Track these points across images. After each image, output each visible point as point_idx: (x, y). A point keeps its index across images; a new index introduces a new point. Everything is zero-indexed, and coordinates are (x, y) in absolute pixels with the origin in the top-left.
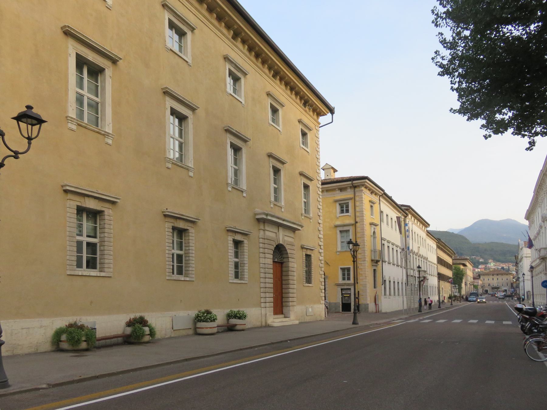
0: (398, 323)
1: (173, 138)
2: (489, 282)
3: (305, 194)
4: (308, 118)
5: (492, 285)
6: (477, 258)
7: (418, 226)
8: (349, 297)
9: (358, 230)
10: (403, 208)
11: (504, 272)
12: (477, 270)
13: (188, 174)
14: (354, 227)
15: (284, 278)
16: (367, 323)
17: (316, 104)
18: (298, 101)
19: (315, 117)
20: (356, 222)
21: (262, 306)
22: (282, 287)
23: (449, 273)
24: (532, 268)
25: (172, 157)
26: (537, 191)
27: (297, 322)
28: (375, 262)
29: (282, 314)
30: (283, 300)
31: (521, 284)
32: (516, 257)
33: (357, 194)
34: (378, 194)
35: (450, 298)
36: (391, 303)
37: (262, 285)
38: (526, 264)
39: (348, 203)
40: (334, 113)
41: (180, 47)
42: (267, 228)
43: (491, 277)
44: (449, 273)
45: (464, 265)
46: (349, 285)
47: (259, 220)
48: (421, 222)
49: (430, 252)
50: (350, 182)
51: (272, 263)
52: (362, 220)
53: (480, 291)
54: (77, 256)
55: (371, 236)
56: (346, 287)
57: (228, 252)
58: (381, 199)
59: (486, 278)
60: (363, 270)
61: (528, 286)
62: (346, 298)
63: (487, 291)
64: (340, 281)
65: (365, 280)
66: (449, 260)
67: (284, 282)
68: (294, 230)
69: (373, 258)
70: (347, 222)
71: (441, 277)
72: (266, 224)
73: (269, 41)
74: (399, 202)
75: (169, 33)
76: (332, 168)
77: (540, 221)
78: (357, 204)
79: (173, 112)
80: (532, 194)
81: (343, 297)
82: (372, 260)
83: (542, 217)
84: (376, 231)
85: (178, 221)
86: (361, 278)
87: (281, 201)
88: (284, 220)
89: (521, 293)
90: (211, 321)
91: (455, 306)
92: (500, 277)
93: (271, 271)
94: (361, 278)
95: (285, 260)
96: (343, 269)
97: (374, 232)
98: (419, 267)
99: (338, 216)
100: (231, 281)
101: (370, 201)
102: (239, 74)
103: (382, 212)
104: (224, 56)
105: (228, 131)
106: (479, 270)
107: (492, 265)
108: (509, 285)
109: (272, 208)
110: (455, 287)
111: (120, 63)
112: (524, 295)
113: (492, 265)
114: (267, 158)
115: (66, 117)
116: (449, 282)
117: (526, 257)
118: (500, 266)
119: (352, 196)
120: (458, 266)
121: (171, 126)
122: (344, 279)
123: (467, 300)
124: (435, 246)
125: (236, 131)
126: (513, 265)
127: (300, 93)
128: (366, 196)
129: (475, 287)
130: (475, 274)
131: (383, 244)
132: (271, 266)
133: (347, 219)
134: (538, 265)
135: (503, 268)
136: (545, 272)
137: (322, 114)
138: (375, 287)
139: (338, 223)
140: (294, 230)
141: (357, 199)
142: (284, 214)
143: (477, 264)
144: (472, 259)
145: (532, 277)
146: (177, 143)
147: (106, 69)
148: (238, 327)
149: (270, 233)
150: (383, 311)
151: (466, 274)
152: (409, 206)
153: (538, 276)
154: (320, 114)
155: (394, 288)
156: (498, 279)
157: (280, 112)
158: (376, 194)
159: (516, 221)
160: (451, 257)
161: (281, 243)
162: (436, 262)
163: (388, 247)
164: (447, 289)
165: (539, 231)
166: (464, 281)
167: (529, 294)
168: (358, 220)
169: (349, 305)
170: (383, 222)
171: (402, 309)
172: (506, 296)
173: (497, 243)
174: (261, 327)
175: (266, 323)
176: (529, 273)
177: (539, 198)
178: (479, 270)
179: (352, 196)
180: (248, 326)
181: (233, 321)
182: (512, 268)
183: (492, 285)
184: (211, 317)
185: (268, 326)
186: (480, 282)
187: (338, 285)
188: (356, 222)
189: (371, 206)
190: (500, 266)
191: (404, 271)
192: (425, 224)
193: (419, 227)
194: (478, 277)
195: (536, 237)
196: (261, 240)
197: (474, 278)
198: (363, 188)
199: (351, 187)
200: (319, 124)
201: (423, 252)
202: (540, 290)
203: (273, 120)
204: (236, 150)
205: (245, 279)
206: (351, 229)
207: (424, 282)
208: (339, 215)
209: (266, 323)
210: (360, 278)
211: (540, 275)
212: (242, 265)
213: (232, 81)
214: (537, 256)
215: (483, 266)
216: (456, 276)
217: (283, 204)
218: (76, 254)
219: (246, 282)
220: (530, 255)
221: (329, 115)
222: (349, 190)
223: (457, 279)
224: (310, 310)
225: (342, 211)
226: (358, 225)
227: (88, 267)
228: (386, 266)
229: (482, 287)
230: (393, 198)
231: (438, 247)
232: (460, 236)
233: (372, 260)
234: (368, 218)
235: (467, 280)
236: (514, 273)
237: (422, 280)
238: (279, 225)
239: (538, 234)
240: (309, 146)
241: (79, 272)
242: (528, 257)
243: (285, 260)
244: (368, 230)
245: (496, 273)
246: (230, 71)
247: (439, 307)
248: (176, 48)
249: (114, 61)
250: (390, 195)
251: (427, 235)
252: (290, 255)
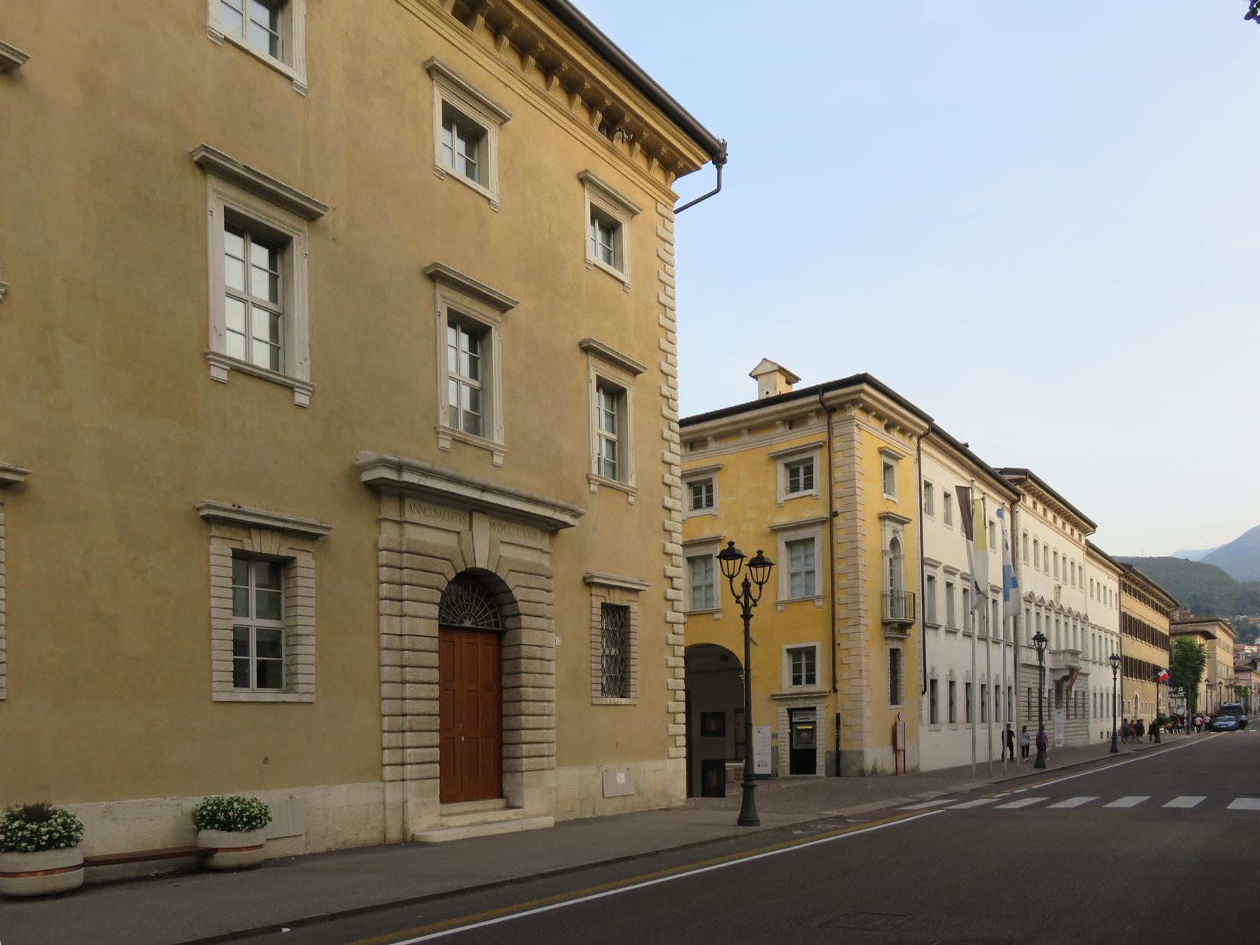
0: (926, 808)
1: (457, 381)
4: (622, 172)
7: (1057, 530)
8: (812, 732)
9: (840, 535)
10: (1006, 477)
12: (1248, 649)
14: (826, 528)
15: (507, 681)
16: (784, 819)
17: (660, 134)
18: (581, 114)
19: (658, 175)
21: (387, 776)
22: (501, 709)
23: (1159, 657)
27: (549, 821)
29: (500, 794)
33: (836, 432)
34: (913, 434)
36: (942, 746)
37: (386, 707)
40: (724, 161)
41: (273, 39)
44: (1159, 657)
45: (1208, 636)
46: (811, 696)
47: (376, 490)
48: (1067, 519)
49: (1102, 604)
50: (816, 398)
51: (436, 633)
54: (235, 661)
55: (884, 552)
58: (923, 445)
60: (852, 652)
62: (804, 735)
64: (787, 686)
65: (856, 682)
66: (1161, 624)
67: (506, 695)
68: (551, 528)
69: (889, 617)
70: (808, 514)
71: (1131, 668)
72: (407, 503)
73: (634, 74)
74: (994, 462)
76: (782, 370)
78: (838, 459)
82: (885, 624)
87: (491, 432)
88: (484, 489)
90: (39, 848)
93: (434, 659)
94: (846, 675)
95: (510, 623)
96: (795, 653)
97: (894, 543)
98: (1039, 638)
99: (780, 500)
100: (216, 697)
101: (882, 452)
103: (928, 485)
105: (207, 166)
109: (444, 451)
110: (1176, 693)
111: (327, 218)
114: (423, 286)
115: (207, 354)
116: (1157, 680)
119: (823, 437)
120: (1188, 638)
121: (451, 352)
122: (797, 681)
123: (1210, 727)
125: (247, 168)
127: (601, 101)
128: (866, 438)
129: (1241, 692)
130: (1242, 657)
131: (931, 578)
132: (434, 644)
133: (810, 507)
137: (680, 164)
138: (894, 700)
139: (782, 519)
140: (551, 528)
141: (837, 444)
142: (502, 470)
143: (1251, 635)
144: (1237, 624)
146: (466, 392)
147: (296, 239)
148: (221, 859)
149: (432, 533)
150: (925, 767)
151: (1212, 657)
152: (1025, 472)
154: (675, 166)
155: (951, 703)
157: (493, 138)
158: (903, 431)
160: (1167, 614)
161: (481, 564)
162: (1117, 631)
163: (994, 601)
166: (1204, 675)
168: (838, 506)
169: (812, 753)
170: (930, 512)
171: (969, 762)
174: (385, 845)
175: (404, 831)
179: (823, 437)
180: (276, 850)
181: (211, 838)
184: (37, 834)
185: (411, 842)
187: (779, 698)
189: (887, 468)
191: (1010, 653)
193: (1043, 519)
196: (384, 557)
197: (1238, 670)
198: (855, 412)
200: (674, 198)
204: (614, 394)
205: (301, 688)
207: (1073, 682)
208: (783, 496)
209: (404, 831)
210: (842, 674)
212: (292, 641)
216: (1181, 664)
217: (632, 483)
218: (231, 656)
219: (305, 698)
221: (709, 168)
222: (814, 421)
223: (1186, 670)
224: (621, 778)
225: (794, 487)
226: (838, 521)
227: (262, 683)
230: (972, 449)
231: (1124, 587)
232: (1206, 566)
233: (885, 624)
234: (870, 496)
235: (1214, 672)
237: (1065, 678)
238: (471, 508)
240: (626, 261)
241: (243, 695)
243: (510, 623)
244: (872, 538)
247: (1114, 749)
248: (258, 43)
249: (309, 215)
250: (961, 440)
251: (1088, 553)
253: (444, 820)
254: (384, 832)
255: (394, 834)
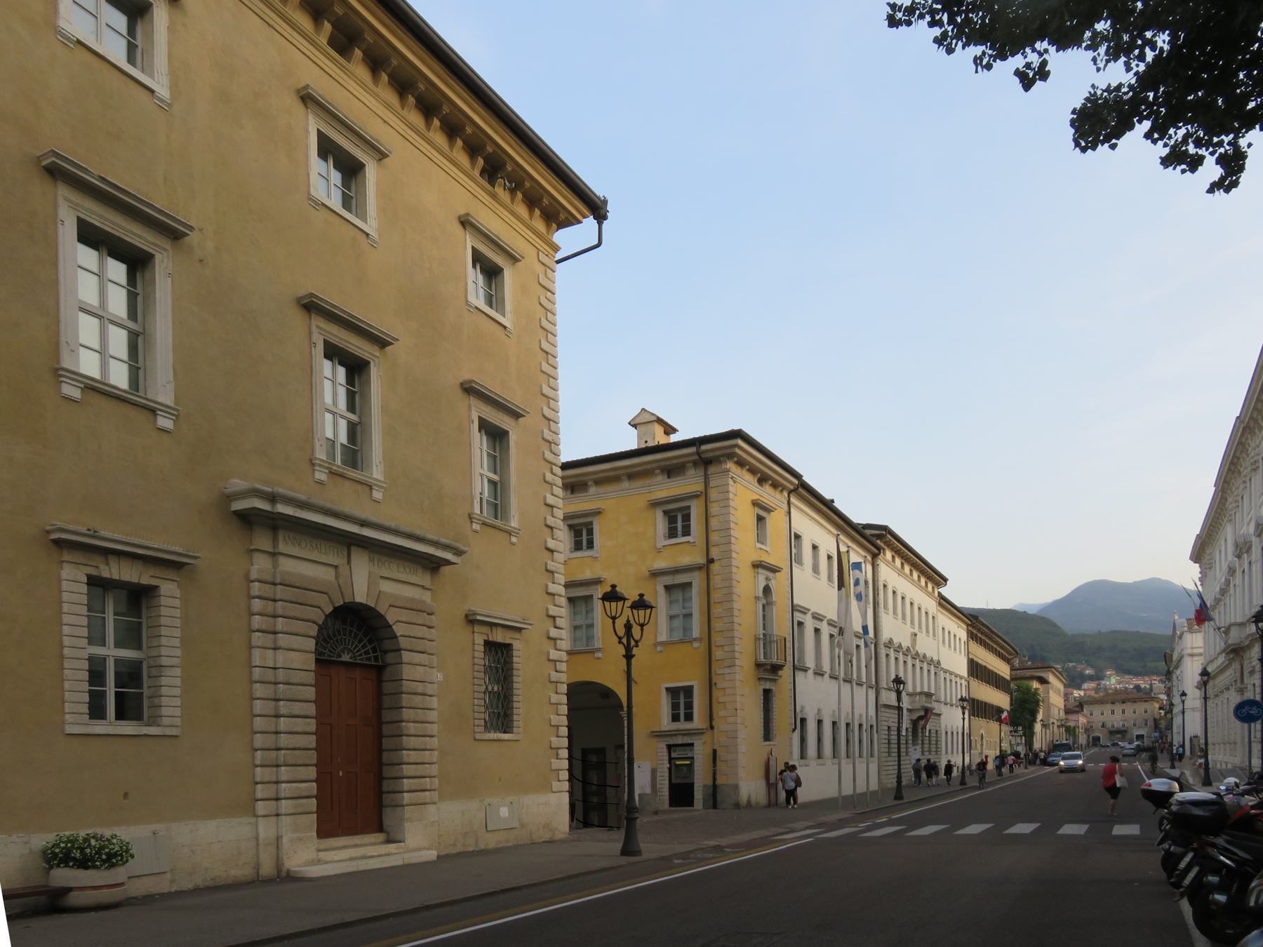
1: (334, 413)
2: (1102, 719)
3: (493, 458)
5: (1109, 725)
6: (1080, 667)
9: (716, 581)
10: (868, 532)
11: (1139, 695)
12: (1076, 693)
13: (59, 391)
17: (555, 194)
19: (540, 225)
20: (711, 561)
23: (1001, 699)
24: (1204, 673)
25: (89, 365)
26: (1225, 481)
27: (431, 855)
28: (769, 670)
29: (380, 829)
30: (384, 789)
31: (1177, 721)
32: (1167, 658)
33: (712, 484)
35: (1002, 758)
38: (1190, 673)
39: (689, 507)
40: (605, 218)
41: (131, 48)
42: (282, 547)
43: (1109, 707)
44: (1001, 699)
45: (1043, 681)
46: (688, 733)
48: (922, 572)
49: (952, 652)
51: (313, 667)
52: (727, 555)
53: (1082, 739)
55: (757, 598)
56: (679, 740)
57: (62, 624)
58: (793, 500)
59: (1097, 710)
61: (1193, 725)
63: (1097, 739)
64: (666, 723)
65: (731, 719)
67: (386, 730)
68: (433, 565)
69: (762, 659)
70: (686, 560)
71: (978, 709)
74: (858, 518)
75: (317, 166)
76: (660, 421)
77: (1230, 557)
78: (714, 509)
79: (332, 352)
80: (1211, 490)
81: (673, 768)
82: (759, 665)
83: (1236, 545)
84: (773, 584)
85: (113, 561)
86: (722, 713)
88: (364, 523)
89: (1177, 740)
91: (1017, 776)
92: (1129, 708)
93: (310, 693)
94: (722, 713)
95: (390, 658)
96: (673, 692)
97: (767, 590)
98: (898, 681)
101: (755, 504)
102: (499, 260)
103: (798, 537)
104: (298, 91)
106: (1082, 693)
107: (1113, 681)
108: (1151, 723)
109: (320, 483)
112: (1183, 746)
113: (1113, 681)
116: (1000, 721)
117: (1192, 655)
118: (1131, 682)
119: (699, 487)
120: (1025, 683)
121: (328, 385)
122: (675, 718)
123: (1045, 762)
124: (962, 634)
125: (103, 179)
126: (1161, 681)
127: (462, 129)
128: (741, 491)
129: (1070, 731)
131: (800, 624)
132: (310, 678)
133: (687, 553)
134: (1222, 671)
135: (1137, 687)
136: (1239, 684)
137: (562, 216)
138: (767, 736)
139: (661, 564)
140: (433, 565)
141: (713, 495)
142: (381, 503)
144: (1067, 670)
145: (1205, 698)
146: (343, 425)
147: (372, 364)
148: (75, 899)
152: (885, 528)
153: (1221, 698)
154: (557, 218)
155: (819, 740)
156: (1123, 712)
158: (775, 485)
159: (1167, 582)
160: (1008, 661)
161: (361, 597)
163: (817, 631)
164: (993, 739)
165: (1228, 582)
167: (1195, 742)
168: (714, 553)
170: (800, 562)
171: (836, 795)
172: (1139, 750)
173: (1126, 632)
174: (257, 881)
175: (279, 865)
176: (1198, 693)
177: (1230, 500)
178: (1082, 693)
181: (64, 876)
182: (1158, 685)
183: (1109, 725)
185: (285, 878)
186: (1082, 720)
187: (659, 735)
188: (711, 561)
189: (760, 519)
190: (1131, 682)
191: (872, 694)
192: (935, 578)
193: (900, 572)
194: (1075, 708)
195: (1217, 601)
197: (1067, 711)
198: (730, 465)
199: (695, 464)
200: (556, 249)
201: (926, 646)
202: (1228, 728)
203: (489, 301)
204: (496, 436)
206: (697, 579)
210: (719, 712)
211: (1226, 695)
212: (154, 672)
213: (480, 277)
214: (1221, 645)
215: (1093, 685)
217: (514, 523)
219: (174, 732)
220: (1201, 651)
221: (590, 222)
222: (691, 472)
223: (1023, 712)
224: (504, 812)
225: (672, 533)
226: (715, 567)
228: (806, 683)
229: (1087, 730)
231: (971, 636)
232: (1042, 618)
233: (759, 665)
235: (1048, 714)
236: (1164, 697)
237: (920, 718)
239: (1223, 592)
240: (508, 306)
242: (1197, 649)
243: (390, 658)
244: (746, 585)
245: (1123, 697)
246: (323, 139)
250: (827, 496)
251: (940, 604)
252: (403, 642)
253: (322, 855)
254: (257, 867)
255: (267, 869)
